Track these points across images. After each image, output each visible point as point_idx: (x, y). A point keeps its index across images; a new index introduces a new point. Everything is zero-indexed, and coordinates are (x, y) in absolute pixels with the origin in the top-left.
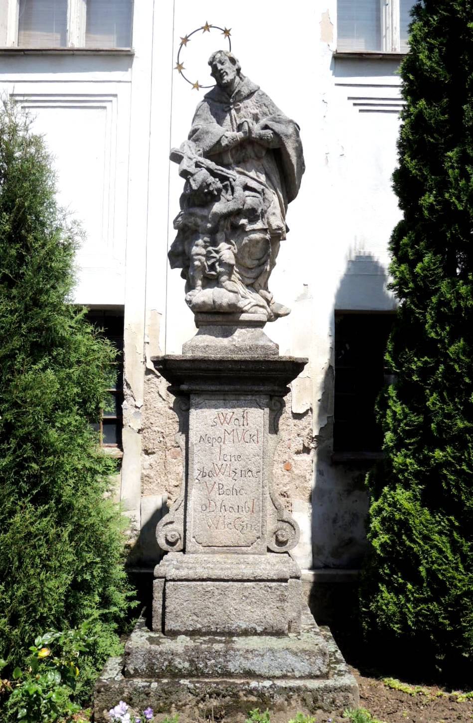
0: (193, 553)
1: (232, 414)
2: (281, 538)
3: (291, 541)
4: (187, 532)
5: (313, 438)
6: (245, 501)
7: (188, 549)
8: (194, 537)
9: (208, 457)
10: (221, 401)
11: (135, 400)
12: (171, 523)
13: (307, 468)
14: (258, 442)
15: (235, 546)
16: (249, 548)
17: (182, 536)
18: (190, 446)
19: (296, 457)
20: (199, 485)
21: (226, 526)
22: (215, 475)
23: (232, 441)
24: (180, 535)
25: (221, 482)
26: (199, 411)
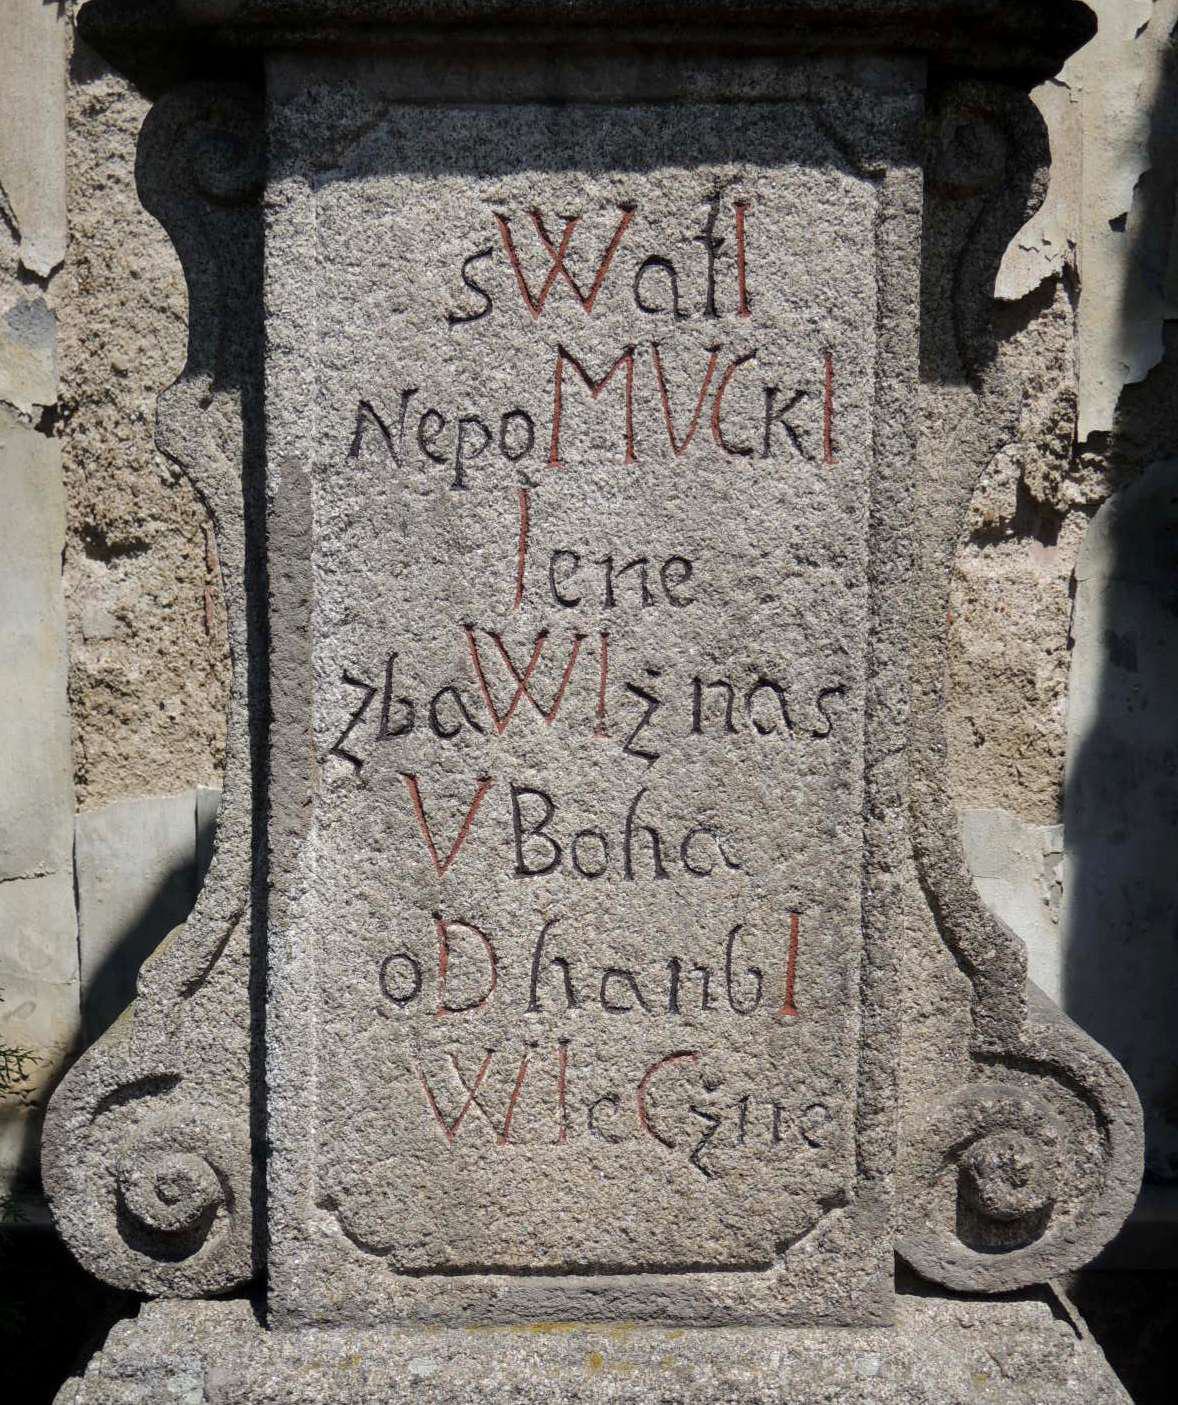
0: (325, 1323)
1: (613, 216)
2: (999, 1193)
3: (1075, 1206)
4: (276, 1163)
5: (1079, 448)
6: (730, 918)
7: (285, 1291)
8: (329, 1203)
9: (425, 576)
10: (529, 113)
11: (16, 236)
12: (158, 1084)
13: (1039, 626)
14: (832, 446)
15: (655, 1268)
16: (758, 1282)
17: (242, 1187)
18: (274, 484)
19: (972, 562)
20: (358, 801)
21: (579, 1118)
22: (485, 717)
23: (617, 437)
24: (223, 1177)
25: (530, 776)
26: (340, 194)
